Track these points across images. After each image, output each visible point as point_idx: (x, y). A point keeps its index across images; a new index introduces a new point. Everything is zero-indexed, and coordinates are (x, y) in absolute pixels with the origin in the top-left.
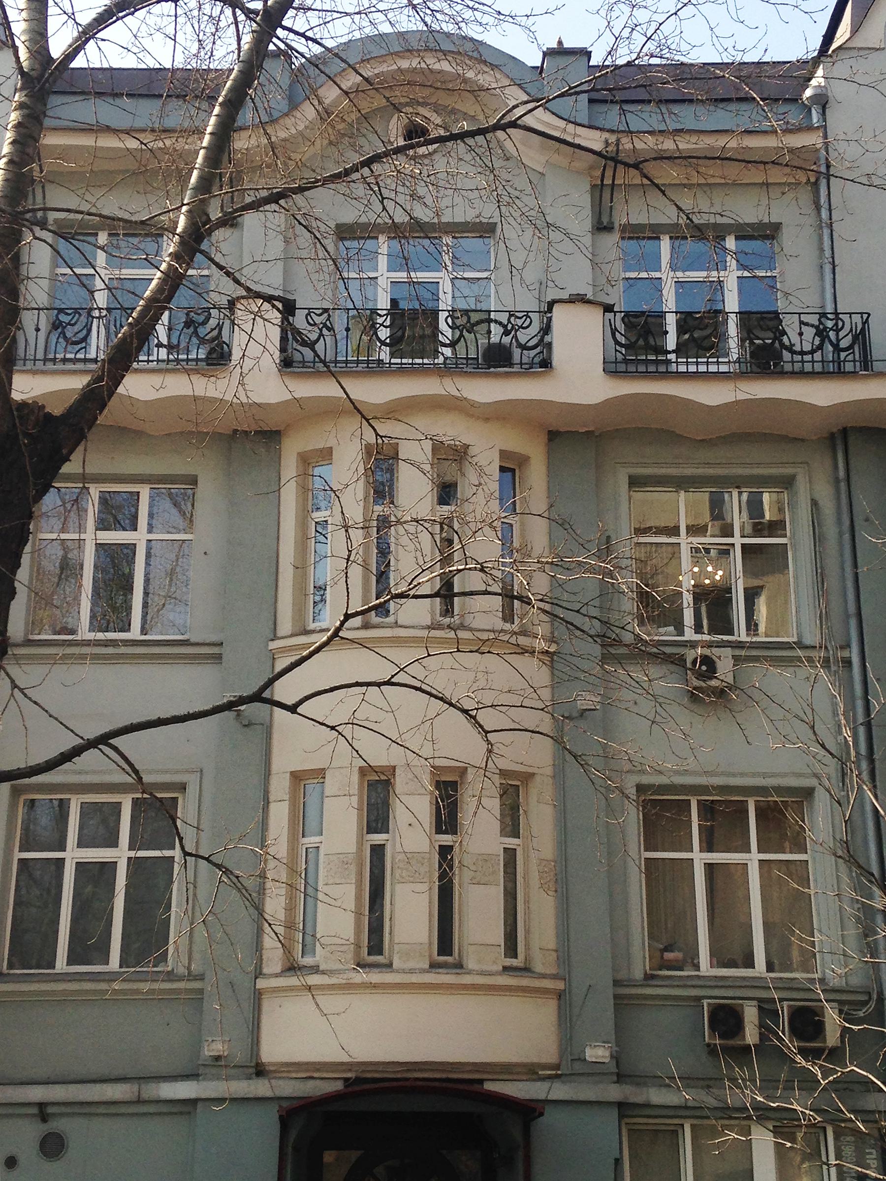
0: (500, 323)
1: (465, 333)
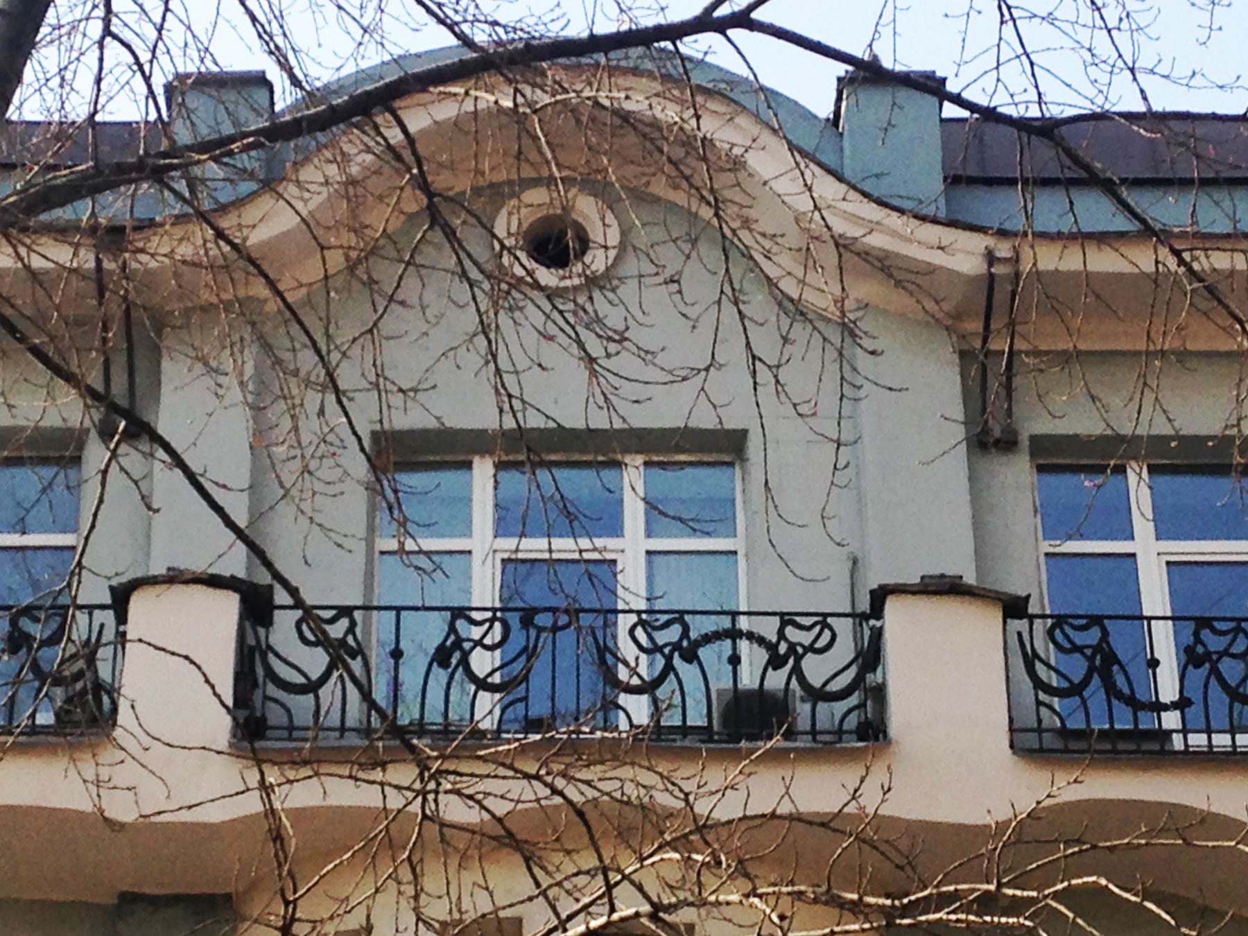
0: (761, 641)
1: (677, 661)
